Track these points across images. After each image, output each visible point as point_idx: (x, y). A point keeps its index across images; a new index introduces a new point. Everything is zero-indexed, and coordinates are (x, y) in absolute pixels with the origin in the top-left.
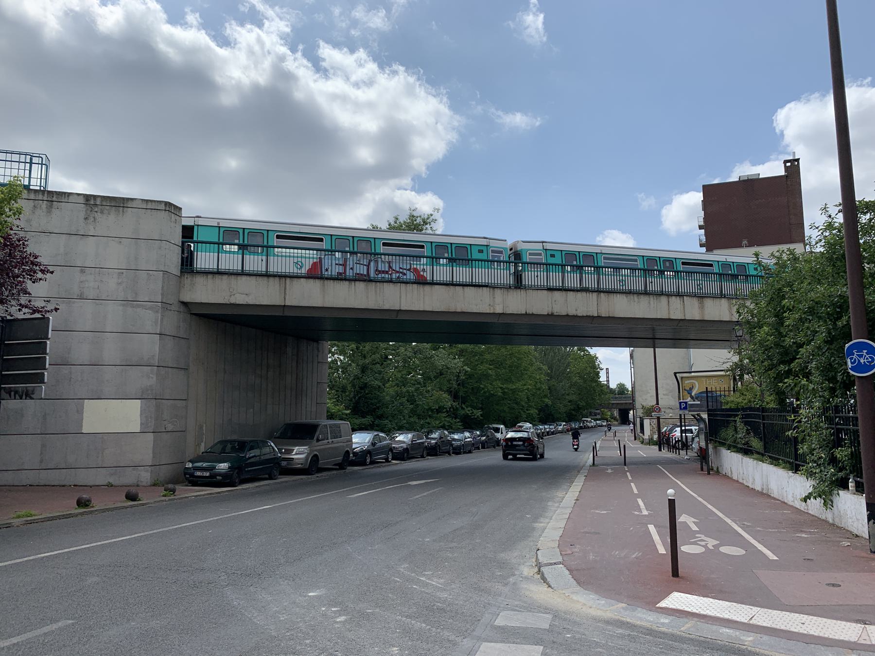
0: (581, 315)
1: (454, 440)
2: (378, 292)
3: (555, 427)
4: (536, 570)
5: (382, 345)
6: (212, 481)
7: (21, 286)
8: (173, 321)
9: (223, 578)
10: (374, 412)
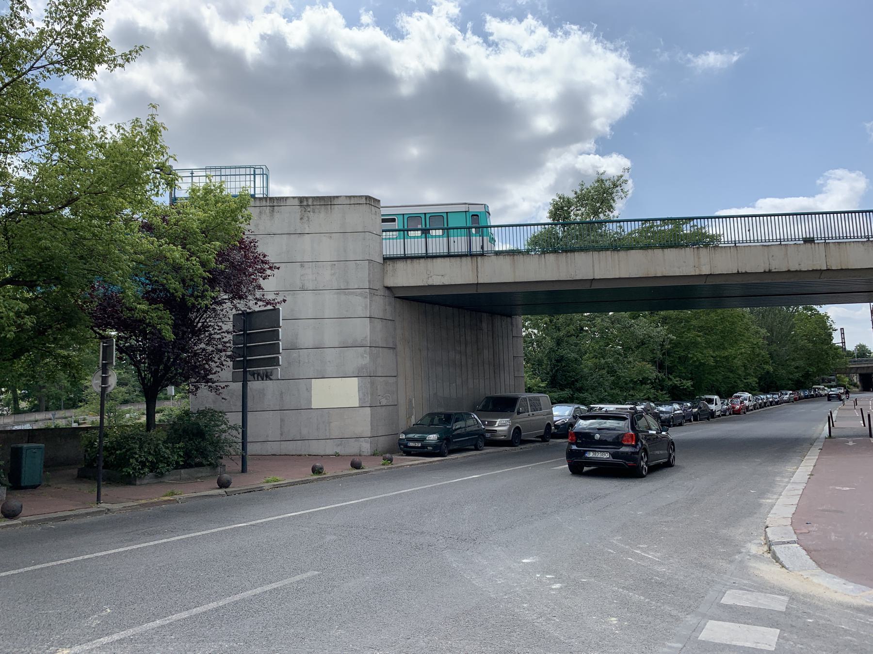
0: (806, 270)
1: (662, 412)
2: (569, 262)
3: (779, 397)
4: (766, 548)
5: (577, 316)
6: (424, 451)
7: (256, 282)
8: (380, 305)
9: (441, 541)
10: (573, 385)
